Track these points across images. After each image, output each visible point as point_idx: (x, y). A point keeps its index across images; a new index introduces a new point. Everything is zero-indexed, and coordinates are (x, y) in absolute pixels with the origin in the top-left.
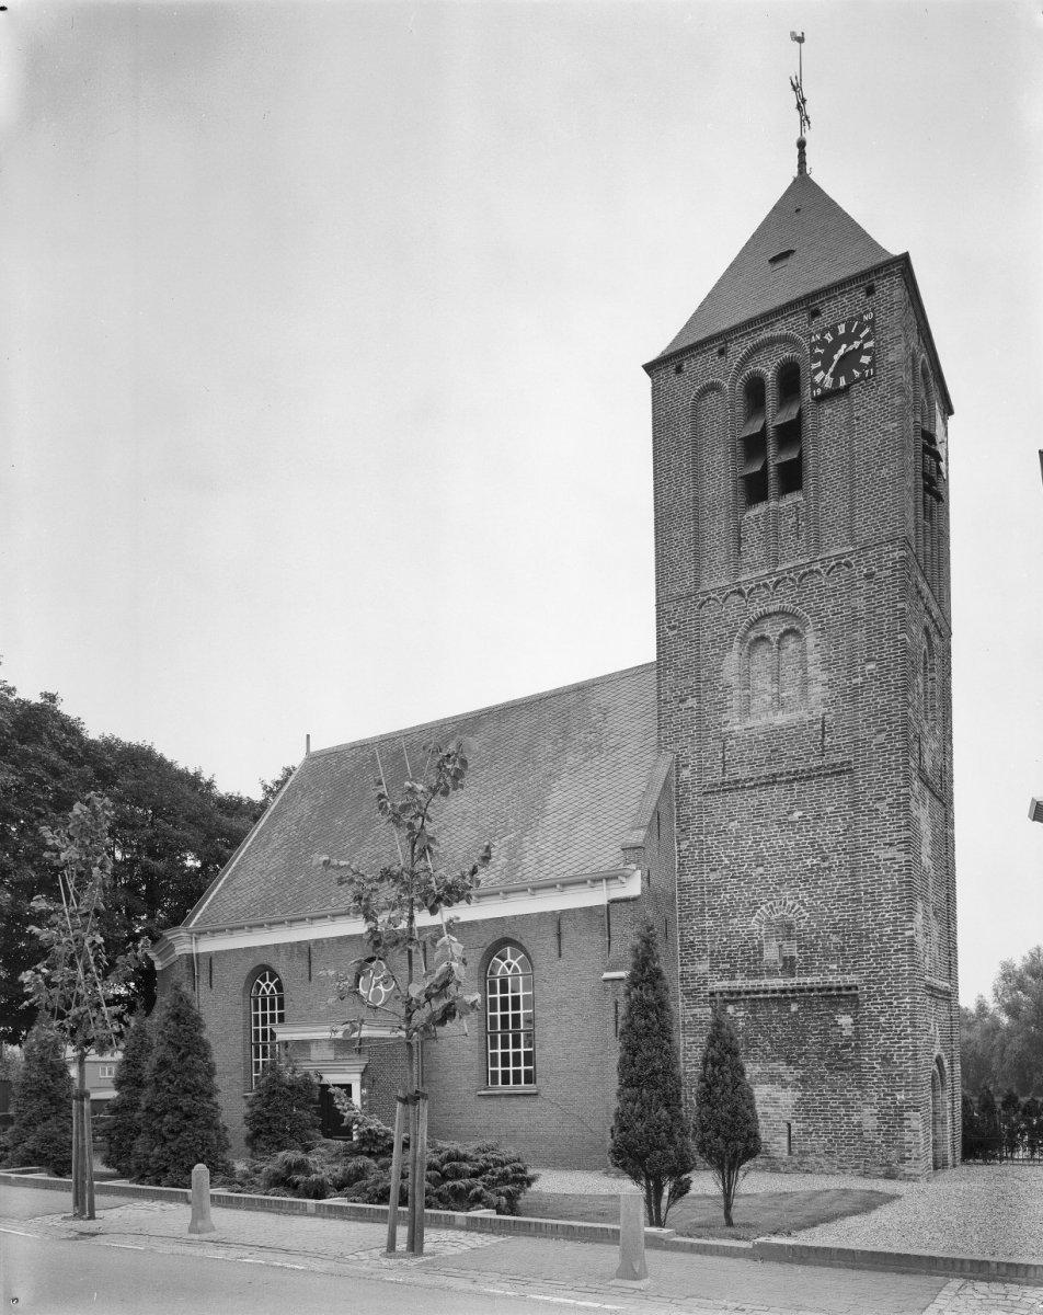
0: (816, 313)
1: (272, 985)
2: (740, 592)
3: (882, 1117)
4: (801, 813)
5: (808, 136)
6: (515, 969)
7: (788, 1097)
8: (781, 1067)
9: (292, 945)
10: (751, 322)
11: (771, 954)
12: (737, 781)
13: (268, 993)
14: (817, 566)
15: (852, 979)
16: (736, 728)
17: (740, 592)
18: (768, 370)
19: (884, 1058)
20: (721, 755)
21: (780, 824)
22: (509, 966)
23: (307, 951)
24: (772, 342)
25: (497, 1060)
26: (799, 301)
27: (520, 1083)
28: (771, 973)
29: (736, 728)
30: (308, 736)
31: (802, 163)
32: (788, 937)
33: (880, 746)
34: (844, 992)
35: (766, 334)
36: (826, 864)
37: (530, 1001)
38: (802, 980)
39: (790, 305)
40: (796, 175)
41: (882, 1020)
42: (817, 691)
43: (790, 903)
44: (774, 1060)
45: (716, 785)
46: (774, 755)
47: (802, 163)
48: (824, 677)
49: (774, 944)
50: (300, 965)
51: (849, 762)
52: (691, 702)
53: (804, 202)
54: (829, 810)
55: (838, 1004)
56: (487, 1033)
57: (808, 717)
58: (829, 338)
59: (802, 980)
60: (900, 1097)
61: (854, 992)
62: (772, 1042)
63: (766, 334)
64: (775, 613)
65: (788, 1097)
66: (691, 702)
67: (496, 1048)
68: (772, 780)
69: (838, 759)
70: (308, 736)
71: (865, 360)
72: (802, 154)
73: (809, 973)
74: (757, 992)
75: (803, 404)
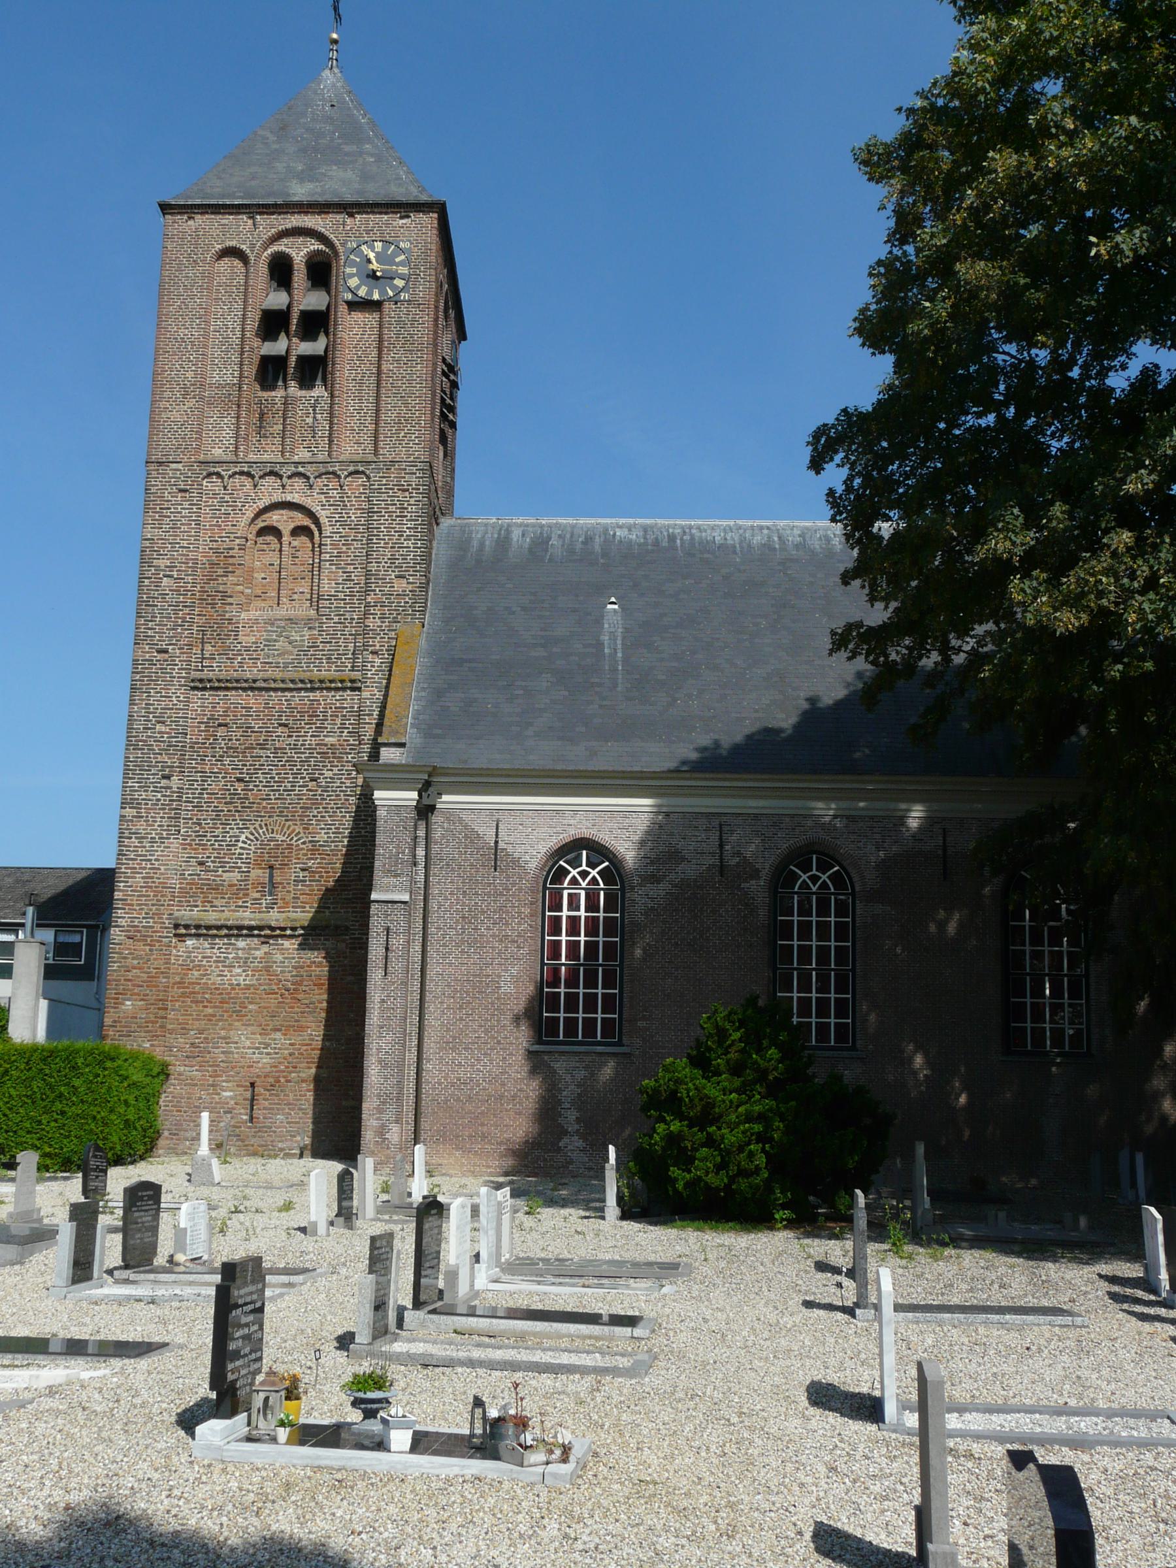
18: (299, 252)
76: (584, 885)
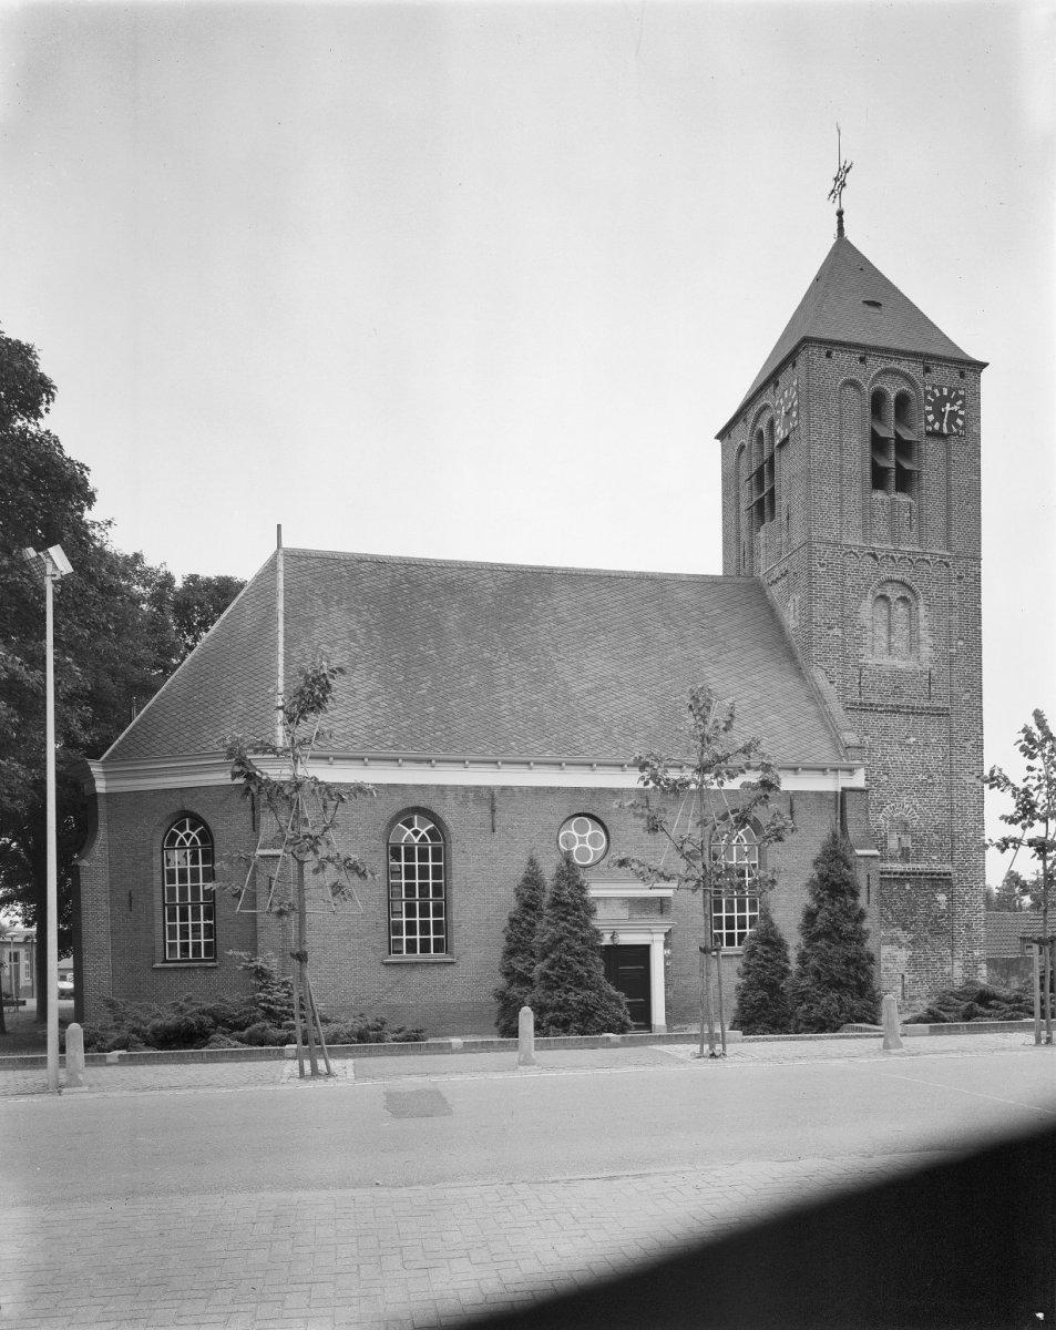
0: (927, 370)
2: (874, 556)
3: (965, 968)
4: (914, 739)
6: (194, 841)
7: (903, 955)
8: (899, 933)
9: (466, 789)
10: (887, 350)
11: (893, 844)
12: (871, 705)
14: (928, 557)
15: (948, 867)
16: (869, 662)
17: (874, 556)
19: (967, 926)
20: (858, 681)
21: (900, 744)
22: (416, 833)
23: (490, 798)
24: (896, 372)
26: (858, 346)
27: (734, 945)
28: (893, 859)
29: (869, 662)
30: (279, 526)
31: (841, 229)
32: (905, 832)
33: (967, 702)
34: (942, 877)
35: (894, 365)
36: (930, 781)
37: (395, 873)
38: (915, 866)
39: (915, 354)
41: (967, 898)
42: (926, 651)
43: (907, 806)
44: (894, 926)
45: (855, 704)
46: (897, 691)
47: (841, 229)
48: (930, 641)
49: (896, 836)
50: (480, 814)
51: (947, 709)
52: (837, 631)
53: (846, 267)
54: (933, 740)
55: (938, 885)
56: (164, 905)
57: (920, 668)
59: (915, 866)
60: (977, 953)
61: (948, 877)
62: (892, 913)
63: (894, 365)
64: (897, 581)
65: (903, 955)
66: (837, 631)
67: (721, 911)
68: (896, 710)
69: (939, 704)
70: (279, 526)
71: (959, 422)
72: (840, 222)
73: (918, 861)
74: (933, 874)
75: (864, 417)
76: (188, 845)
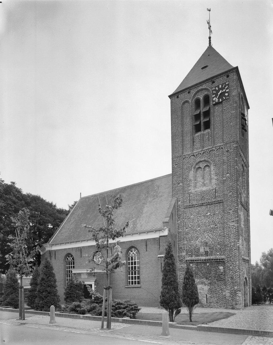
1: (71, 258)
5: (211, 36)
6: (135, 254)
13: (70, 261)
18: (201, 97)
25: (130, 278)
30: (81, 193)
31: (210, 43)
35: (200, 88)
40: (208, 46)
47: (210, 43)
56: (127, 271)
58: (217, 89)
63: (200, 88)
70: (81, 193)
71: (226, 94)
72: (210, 41)
